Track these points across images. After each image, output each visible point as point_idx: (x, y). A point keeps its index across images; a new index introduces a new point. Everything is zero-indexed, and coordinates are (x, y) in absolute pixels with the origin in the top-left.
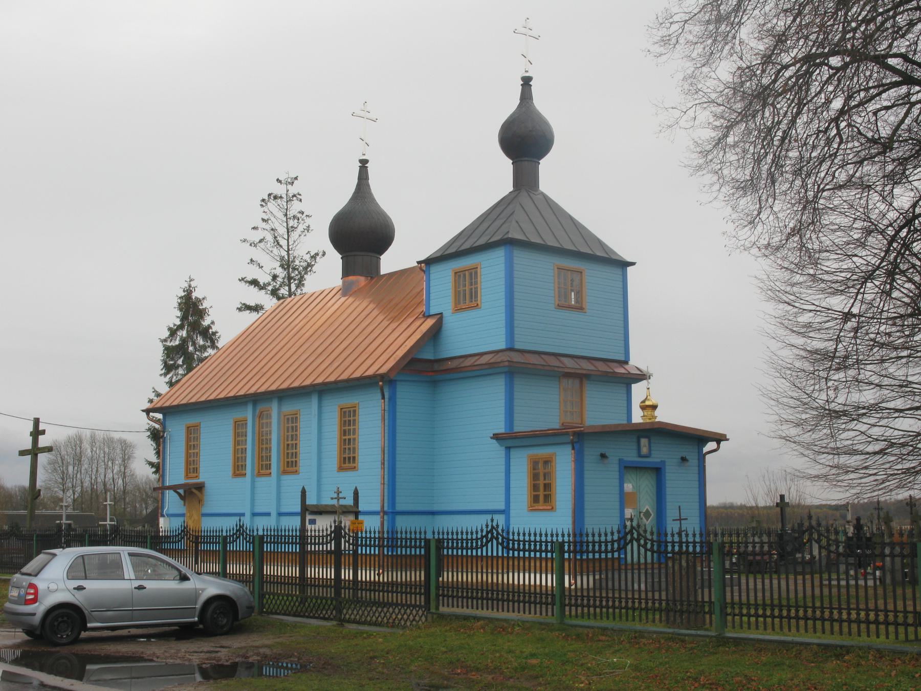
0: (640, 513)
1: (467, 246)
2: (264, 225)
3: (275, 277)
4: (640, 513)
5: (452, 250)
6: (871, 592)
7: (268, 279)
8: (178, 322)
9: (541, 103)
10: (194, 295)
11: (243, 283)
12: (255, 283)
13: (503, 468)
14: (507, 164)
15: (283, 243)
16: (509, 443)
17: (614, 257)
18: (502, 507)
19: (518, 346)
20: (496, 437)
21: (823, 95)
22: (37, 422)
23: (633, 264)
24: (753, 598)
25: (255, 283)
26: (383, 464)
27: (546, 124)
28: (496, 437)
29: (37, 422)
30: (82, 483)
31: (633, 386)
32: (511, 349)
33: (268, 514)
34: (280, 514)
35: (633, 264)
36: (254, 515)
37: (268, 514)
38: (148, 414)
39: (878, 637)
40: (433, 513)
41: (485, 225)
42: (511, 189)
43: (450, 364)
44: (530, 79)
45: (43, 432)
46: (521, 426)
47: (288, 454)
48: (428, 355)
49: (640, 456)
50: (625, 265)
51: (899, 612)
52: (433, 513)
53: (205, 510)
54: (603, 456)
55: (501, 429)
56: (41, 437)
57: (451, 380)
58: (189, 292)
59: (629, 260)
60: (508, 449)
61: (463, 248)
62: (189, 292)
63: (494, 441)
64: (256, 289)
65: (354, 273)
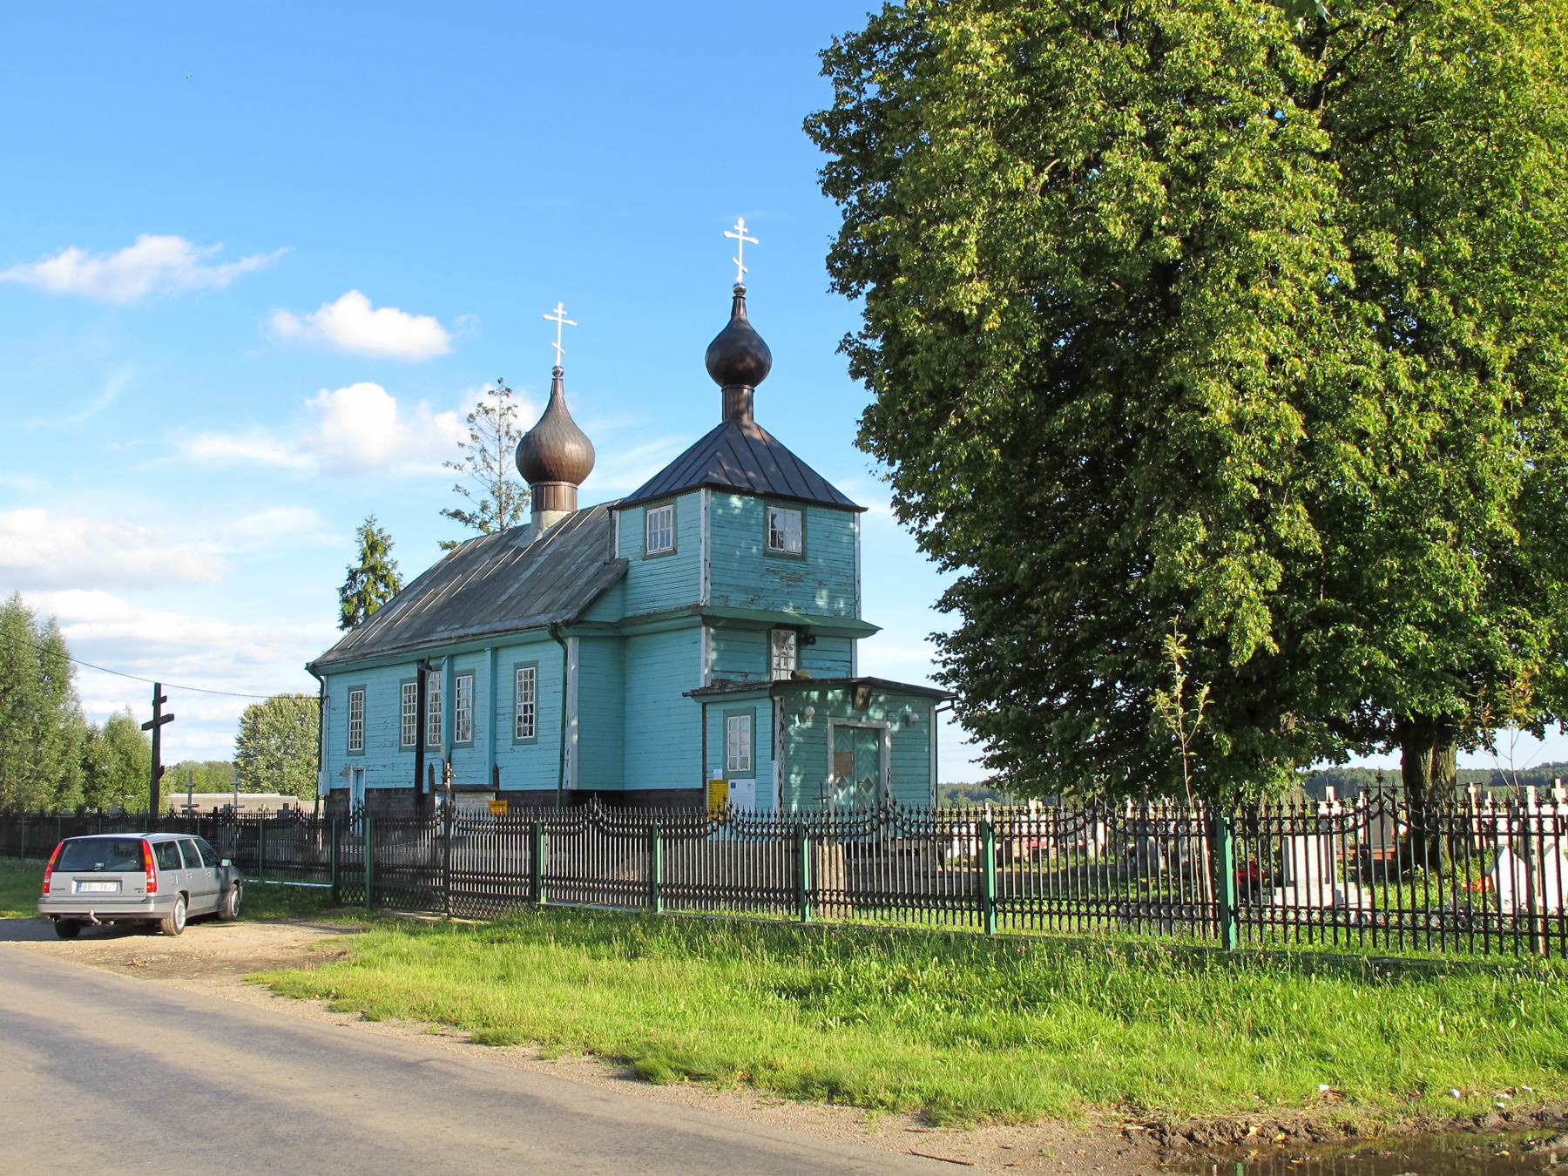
1: (662, 490)
2: (473, 443)
3: (484, 508)
5: (647, 495)
7: (477, 509)
9: (754, 318)
11: (444, 517)
12: (457, 514)
14: (715, 391)
15: (495, 466)
16: (705, 699)
17: (840, 501)
22: (158, 687)
23: (865, 509)
25: (457, 514)
27: (762, 344)
29: (158, 687)
30: (1088, 964)
31: (860, 641)
35: (865, 509)
39: (1487, 952)
41: (680, 471)
42: (719, 420)
44: (743, 291)
45: (165, 699)
47: (531, 722)
50: (855, 509)
51: (1505, 915)
56: (163, 705)
59: (860, 504)
61: (658, 492)
64: (462, 524)
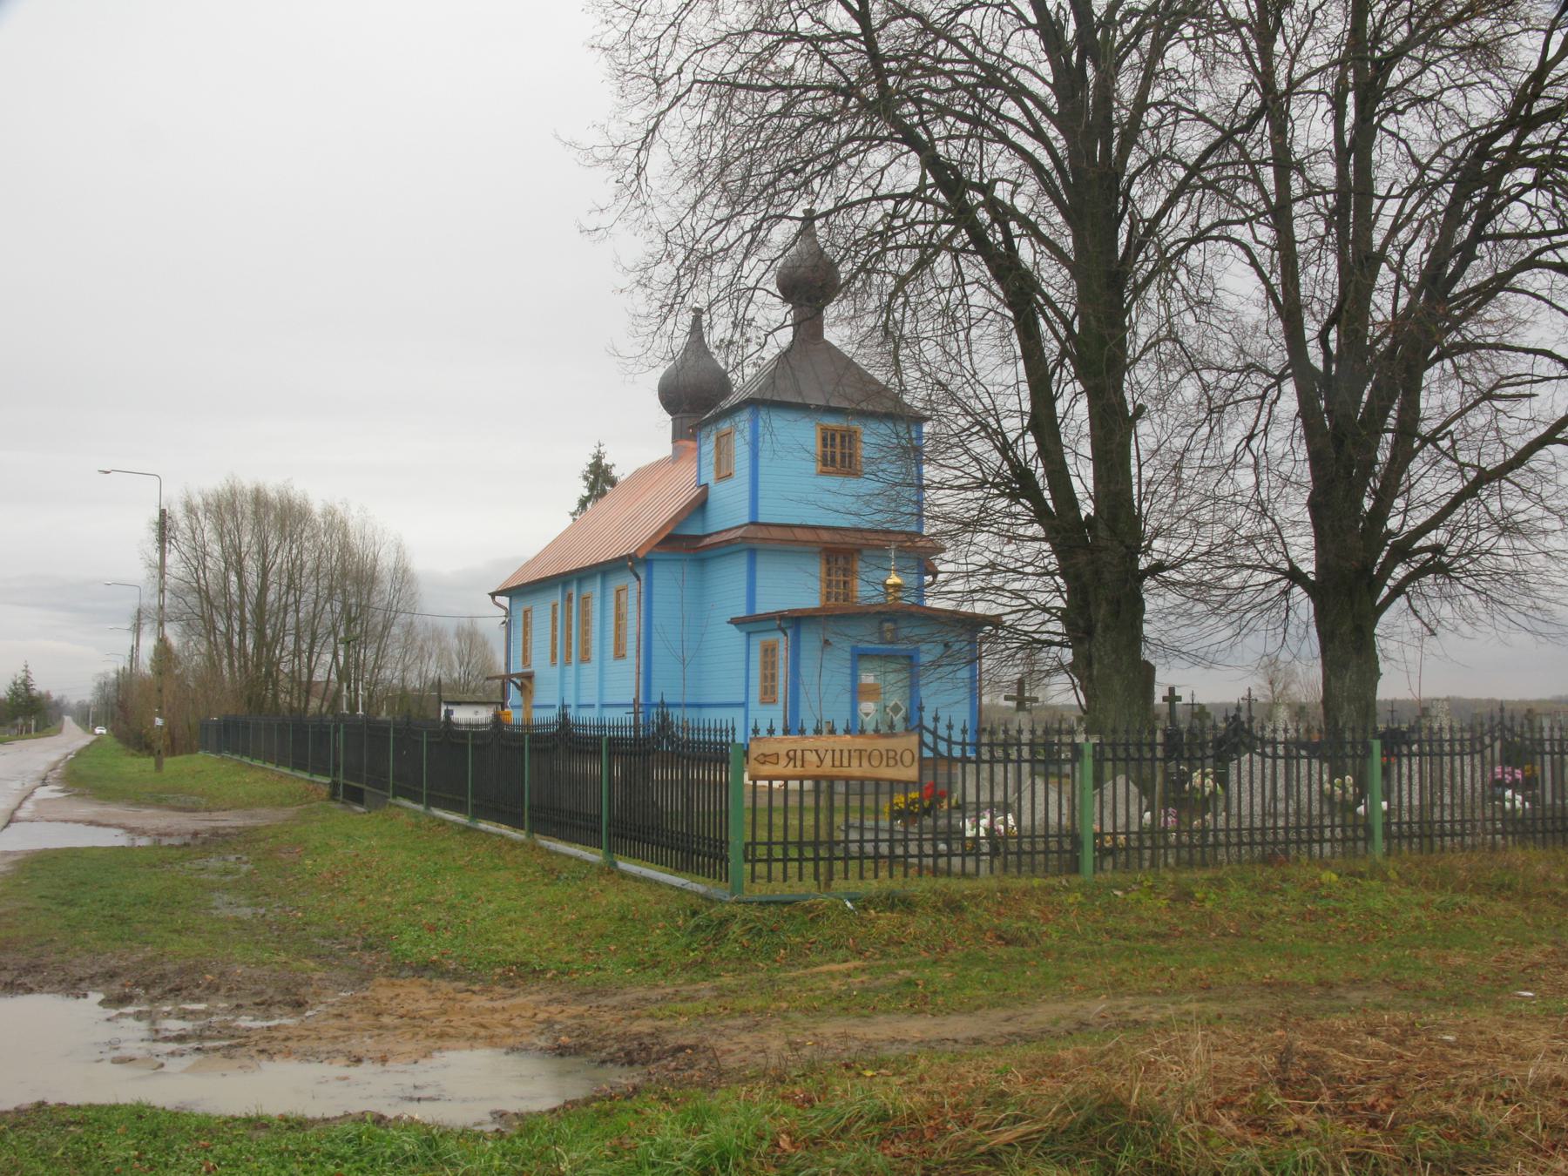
0: (885, 707)
4: (885, 707)
6: (793, 801)
8: (586, 493)
10: (604, 462)
13: (743, 656)
16: (751, 627)
18: (742, 699)
19: (761, 519)
20: (736, 622)
21: (1224, 174)
24: (1306, 800)
26: (638, 651)
28: (736, 622)
32: (754, 523)
33: (592, 706)
34: (603, 706)
36: (579, 706)
37: (592, 706)
38: (493, 598)
40: (700, 706)
43: (707, 541)
46: (762, 608)
48: (694, 530)
49: (883, 641)
52: (700, 706)
53: (536, 701)
54: (826, 642)
55: (742, 612)
57: (724, 555)
58: (598, 457)
60: (749, 634)
62: (598, 457)
63: (733, 627)
65: (681, 438)
